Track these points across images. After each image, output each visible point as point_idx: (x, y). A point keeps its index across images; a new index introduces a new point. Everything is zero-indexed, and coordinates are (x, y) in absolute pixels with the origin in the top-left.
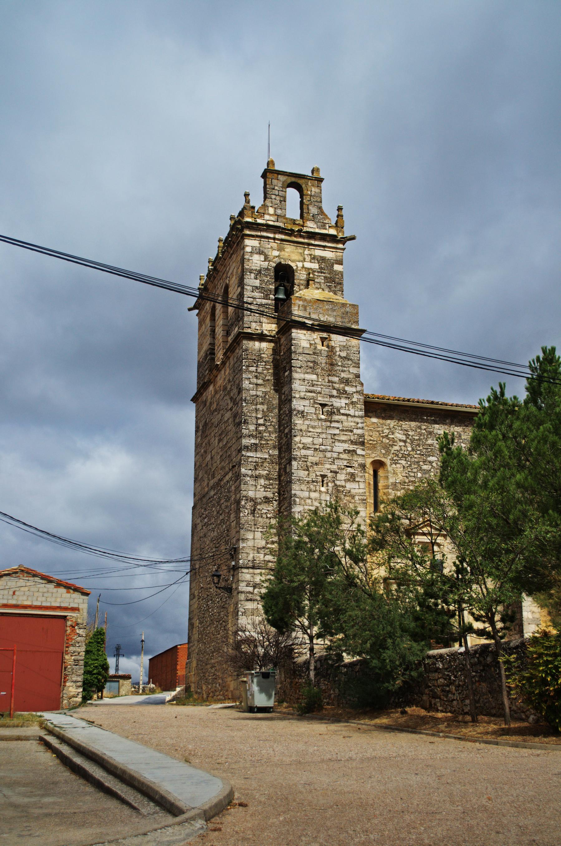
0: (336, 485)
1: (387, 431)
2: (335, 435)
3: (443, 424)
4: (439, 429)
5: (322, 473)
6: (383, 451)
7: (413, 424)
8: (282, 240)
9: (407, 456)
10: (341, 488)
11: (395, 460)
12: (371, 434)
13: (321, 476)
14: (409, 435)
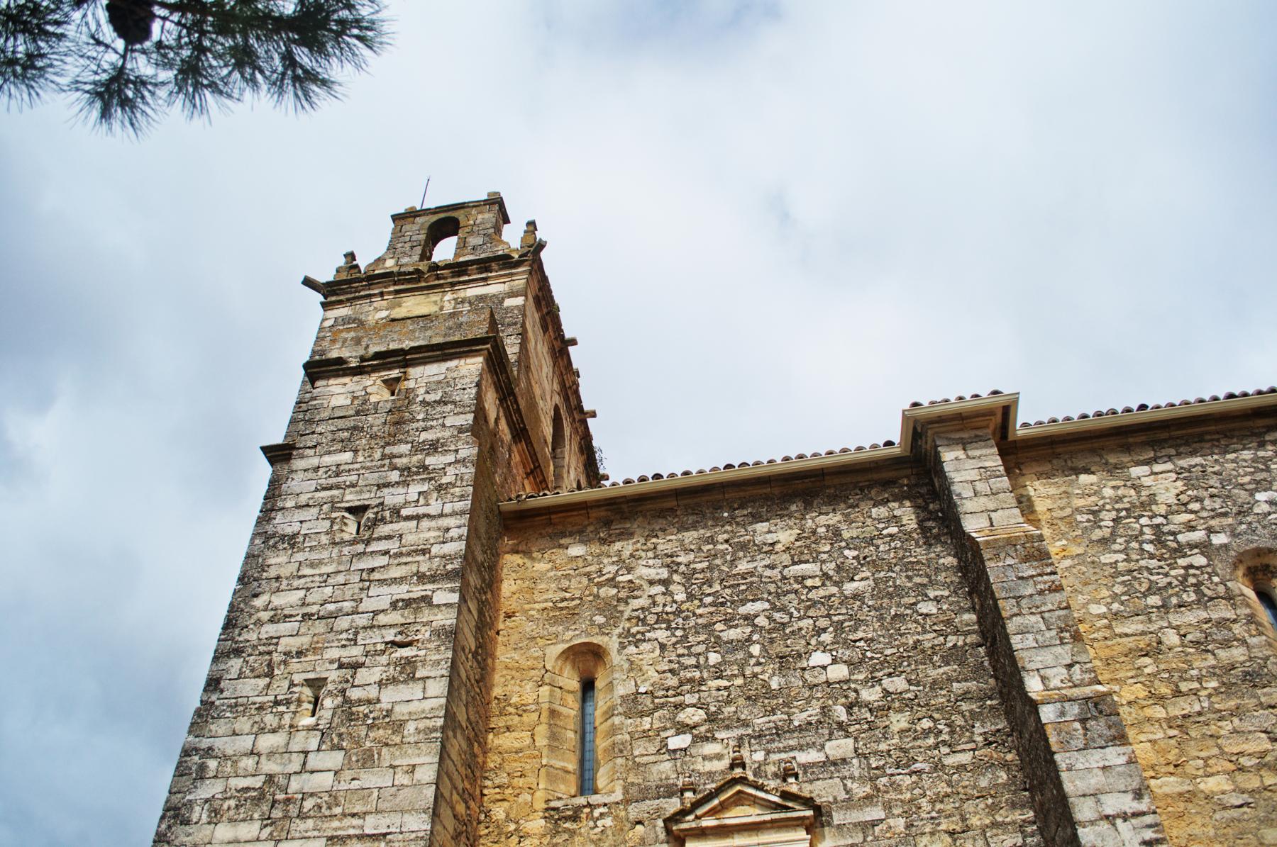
0: (347, 701)
1: (613, 569)
2: (373, 570)
3: (781, 516)
4: (769, 532)
5: (312, 676)
6: (600, 619)
7: (690, 536)
8: (397, 292)
9: (672, 617)
10: (361, 709)
11: (634, 635)
12: (565, 583)
13: (309, 683)
14: (679, 564)
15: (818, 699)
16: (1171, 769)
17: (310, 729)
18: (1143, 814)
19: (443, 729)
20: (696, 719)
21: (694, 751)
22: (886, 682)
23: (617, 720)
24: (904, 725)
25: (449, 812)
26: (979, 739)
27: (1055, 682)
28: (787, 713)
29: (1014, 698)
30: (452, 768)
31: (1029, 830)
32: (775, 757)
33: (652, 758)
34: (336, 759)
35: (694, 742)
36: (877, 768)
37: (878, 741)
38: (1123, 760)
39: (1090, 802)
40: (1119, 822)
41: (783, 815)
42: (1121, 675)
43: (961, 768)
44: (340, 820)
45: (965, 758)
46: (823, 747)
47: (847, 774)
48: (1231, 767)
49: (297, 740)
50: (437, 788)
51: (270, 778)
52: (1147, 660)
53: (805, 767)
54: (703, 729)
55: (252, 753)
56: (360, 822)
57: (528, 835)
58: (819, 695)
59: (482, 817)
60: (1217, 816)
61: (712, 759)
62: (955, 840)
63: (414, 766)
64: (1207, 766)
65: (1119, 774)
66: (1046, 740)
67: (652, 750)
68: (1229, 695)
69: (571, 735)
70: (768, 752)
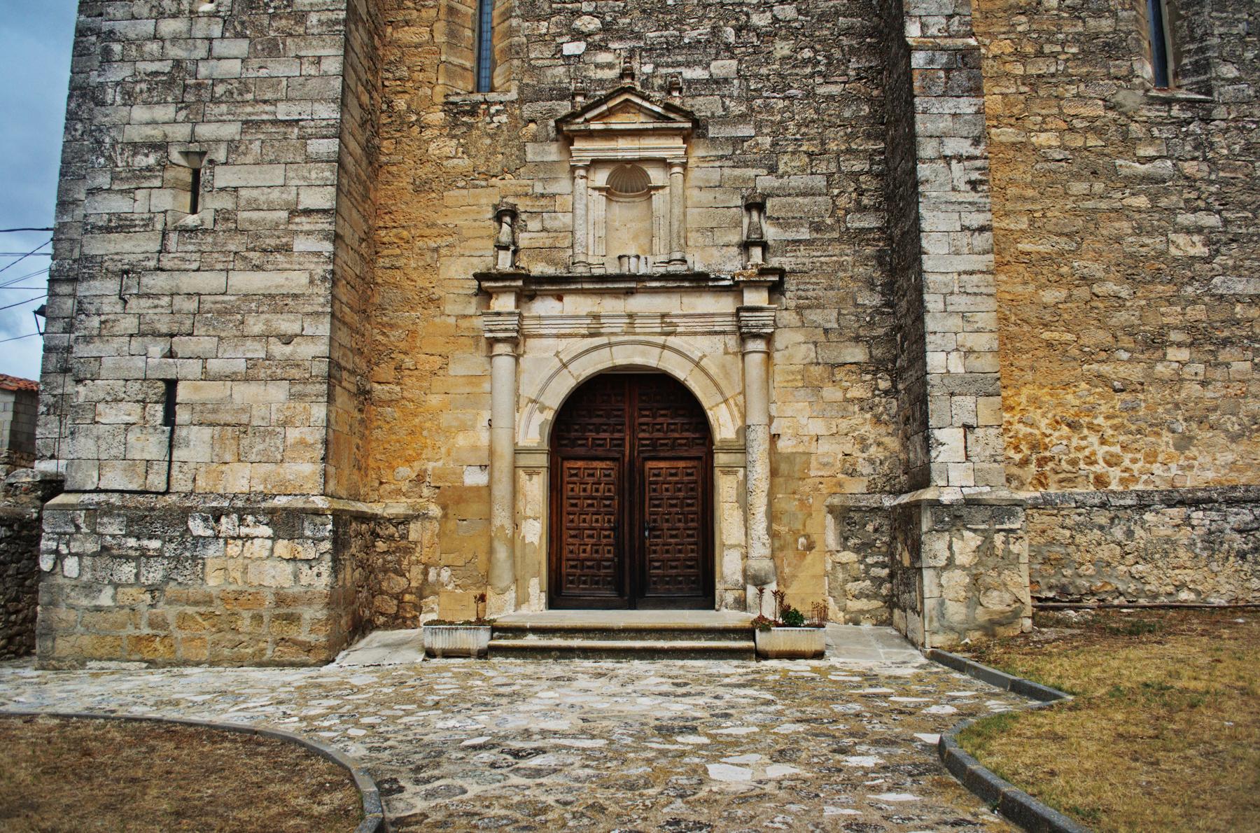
15: (710, 19)
16: (1013, 121)
17: (212, 15)
18: (976, 158)
19: (345, 22)
20: (591, 27)
21: (587, 58)
22: (777, 9)
23: (514, 22)
24: (786, 52)
25: (355, 102)
26: (852, 73)
27: (933, 31)
28: (679, 30)
29: (893, 40)
30: (356, 61)
31: (877, 158)
32: (663, 71)
33: (547, 62)
34: (242, 47)
35: (587, 49)
36: (755, 90)
37: (760, 65)
38: (972, 109)
39: (934, 142)
40: (954, 162)
41: (664, 125)
42: (995, 29)
43: (830, 98)
44: (252, 106)
45: (835, 89)
46: (708, 65)
47: (727, 93)
48: (1064, 126)
49: (198, 26)
50: (344, 79)
51: (178, 63)
52: (1023, 19)
53: (690, 83)
54: (597, 38)
55: (155, 38)
56: (272, 108)
57: (428, 126)
58: (712, 15)
59: (384, 107)
60: (1038, 166)
61: (605, 66)
62: (812, 161)
63: (320, 57)
64: (1044, 122)
65: (966, 122)
66: (911, 83)
67: (548, 54)
68: (1084, 62)
69: (468, 33)
70: (657, 66)
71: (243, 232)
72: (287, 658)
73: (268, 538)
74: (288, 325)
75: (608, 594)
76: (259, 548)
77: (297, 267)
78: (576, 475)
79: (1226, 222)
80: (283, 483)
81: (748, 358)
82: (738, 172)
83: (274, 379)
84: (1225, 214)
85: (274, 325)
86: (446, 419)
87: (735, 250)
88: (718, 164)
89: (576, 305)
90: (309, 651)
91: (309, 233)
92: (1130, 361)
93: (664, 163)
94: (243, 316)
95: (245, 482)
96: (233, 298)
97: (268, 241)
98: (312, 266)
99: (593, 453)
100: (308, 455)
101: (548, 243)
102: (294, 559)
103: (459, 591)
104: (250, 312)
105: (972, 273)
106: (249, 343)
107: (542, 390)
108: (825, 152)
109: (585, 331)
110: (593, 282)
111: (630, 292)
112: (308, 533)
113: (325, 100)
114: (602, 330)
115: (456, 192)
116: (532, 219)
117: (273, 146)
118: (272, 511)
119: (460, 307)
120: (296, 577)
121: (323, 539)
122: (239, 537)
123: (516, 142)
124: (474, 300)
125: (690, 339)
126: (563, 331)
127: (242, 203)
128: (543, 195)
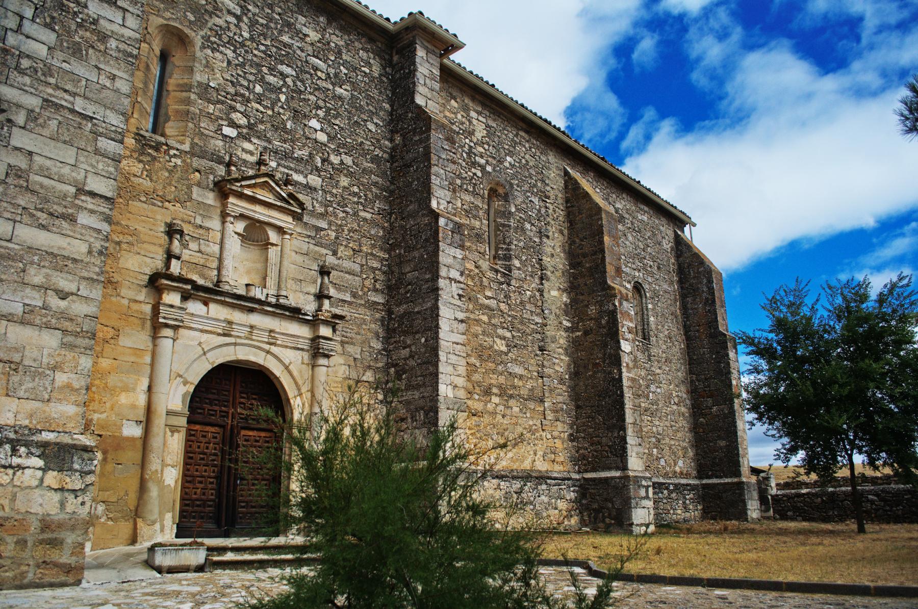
21: (237, 142)
24: (346, 184)
33: (211, 134)
34: (50, 37)
41: (286, 206)
43: (365, 219)
44: (54, 89)
45: (368, 216)
56: (71, 99)
67: (212, 128)
70: (279, 165)
71: (33, 192)
72: (47, 579)
73: (40, 469)
74: (65, 283)
75: (211, 526)
76: (29, 477)
77: (79, 236)
78: (193, 435)
79: (513, 337)
80: (48, 420)
81: (316, 369)
82: (317, 248)
83: (48, 327)
84: (514, 333)
85: (54, 280)
86: (112, 380)
87: (312, 298)
88: (307, 240)
89: (217, 311)
90: (68, 572)
91: (92, 212)
92: (479, 400)
93: (280, 230)
94: (25, 265)
95: (10, 415)
96: (17, 247)
97: (55, 207)
98: (92, 240)
99: (207, 420)
100: (73, 398)
101: (202, 262)
102: (62, 490)
103: (110, 523)
104: (32, 263)
105: (457, 344)
106: (28, 290)
107: (187, 369)
108: (360, 251)
109: (220, 331)
110: (232, 298)
111: (251, 310)
112: (76, 466)
113: (116, 111)
114: (232, 333)
115: (139, 204)
116: (193, 241)
117: (68, 130)
118: (45, 445)
119: (133, 293)
120: (62, 504)
121: (90, 472)
122: (11, 467)
123: (186, 182)
124: (144, 290)
125: (281, 349)
126: (206, 328)
127: (36, 167)
128: (201, 227)
